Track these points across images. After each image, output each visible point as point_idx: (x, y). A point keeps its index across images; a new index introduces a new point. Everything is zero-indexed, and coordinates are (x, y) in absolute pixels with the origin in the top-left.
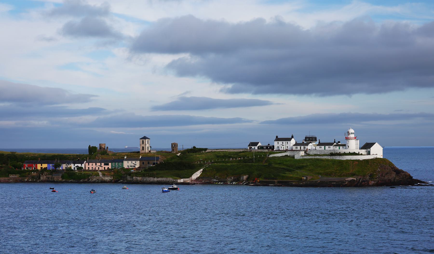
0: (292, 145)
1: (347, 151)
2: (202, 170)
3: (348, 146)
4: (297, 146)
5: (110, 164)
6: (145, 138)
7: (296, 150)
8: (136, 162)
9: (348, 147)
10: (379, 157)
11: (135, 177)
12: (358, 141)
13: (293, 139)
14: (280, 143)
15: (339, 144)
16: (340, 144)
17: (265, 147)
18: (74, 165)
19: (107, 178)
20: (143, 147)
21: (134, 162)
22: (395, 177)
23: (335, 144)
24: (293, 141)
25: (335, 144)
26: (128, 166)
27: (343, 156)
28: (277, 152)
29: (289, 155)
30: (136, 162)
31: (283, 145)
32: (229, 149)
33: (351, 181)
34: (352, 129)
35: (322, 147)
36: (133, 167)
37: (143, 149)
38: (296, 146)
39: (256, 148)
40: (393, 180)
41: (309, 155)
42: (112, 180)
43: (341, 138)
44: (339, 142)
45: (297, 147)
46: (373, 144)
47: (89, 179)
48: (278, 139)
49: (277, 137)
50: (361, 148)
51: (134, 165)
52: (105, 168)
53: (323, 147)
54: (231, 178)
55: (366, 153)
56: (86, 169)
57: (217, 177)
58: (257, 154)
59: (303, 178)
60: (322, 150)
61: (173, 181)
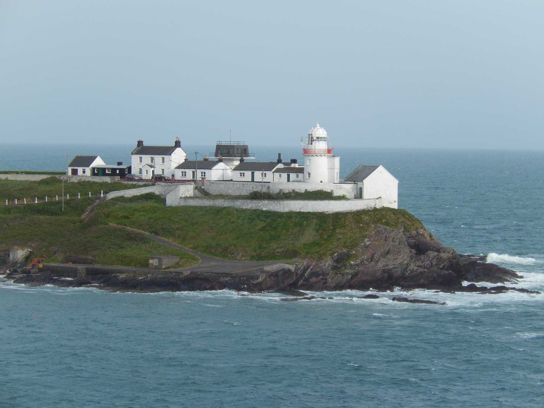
0: (174, 165)
1: (301, 187)
3: (309, 174)
4: (289, 174)
9: (309, 176)
10: (386, 205)
12: (337, 160)
14: (147, 159)
15: (293, 165)
16: (297, 166)
17: (110, 168)
23: (280, 166)
25: (280, 166)
27: (282, 202)
28: (132, 185)
29: (157, 193)
32: (369, 199)
33: (275, 275)
34: (321, 126)
38: (183, 170)
45: (185, 173)
46: (375, 168)
49: (140, 143)
53: (248, 175)
58: (84, 185)
59: (151, 261)
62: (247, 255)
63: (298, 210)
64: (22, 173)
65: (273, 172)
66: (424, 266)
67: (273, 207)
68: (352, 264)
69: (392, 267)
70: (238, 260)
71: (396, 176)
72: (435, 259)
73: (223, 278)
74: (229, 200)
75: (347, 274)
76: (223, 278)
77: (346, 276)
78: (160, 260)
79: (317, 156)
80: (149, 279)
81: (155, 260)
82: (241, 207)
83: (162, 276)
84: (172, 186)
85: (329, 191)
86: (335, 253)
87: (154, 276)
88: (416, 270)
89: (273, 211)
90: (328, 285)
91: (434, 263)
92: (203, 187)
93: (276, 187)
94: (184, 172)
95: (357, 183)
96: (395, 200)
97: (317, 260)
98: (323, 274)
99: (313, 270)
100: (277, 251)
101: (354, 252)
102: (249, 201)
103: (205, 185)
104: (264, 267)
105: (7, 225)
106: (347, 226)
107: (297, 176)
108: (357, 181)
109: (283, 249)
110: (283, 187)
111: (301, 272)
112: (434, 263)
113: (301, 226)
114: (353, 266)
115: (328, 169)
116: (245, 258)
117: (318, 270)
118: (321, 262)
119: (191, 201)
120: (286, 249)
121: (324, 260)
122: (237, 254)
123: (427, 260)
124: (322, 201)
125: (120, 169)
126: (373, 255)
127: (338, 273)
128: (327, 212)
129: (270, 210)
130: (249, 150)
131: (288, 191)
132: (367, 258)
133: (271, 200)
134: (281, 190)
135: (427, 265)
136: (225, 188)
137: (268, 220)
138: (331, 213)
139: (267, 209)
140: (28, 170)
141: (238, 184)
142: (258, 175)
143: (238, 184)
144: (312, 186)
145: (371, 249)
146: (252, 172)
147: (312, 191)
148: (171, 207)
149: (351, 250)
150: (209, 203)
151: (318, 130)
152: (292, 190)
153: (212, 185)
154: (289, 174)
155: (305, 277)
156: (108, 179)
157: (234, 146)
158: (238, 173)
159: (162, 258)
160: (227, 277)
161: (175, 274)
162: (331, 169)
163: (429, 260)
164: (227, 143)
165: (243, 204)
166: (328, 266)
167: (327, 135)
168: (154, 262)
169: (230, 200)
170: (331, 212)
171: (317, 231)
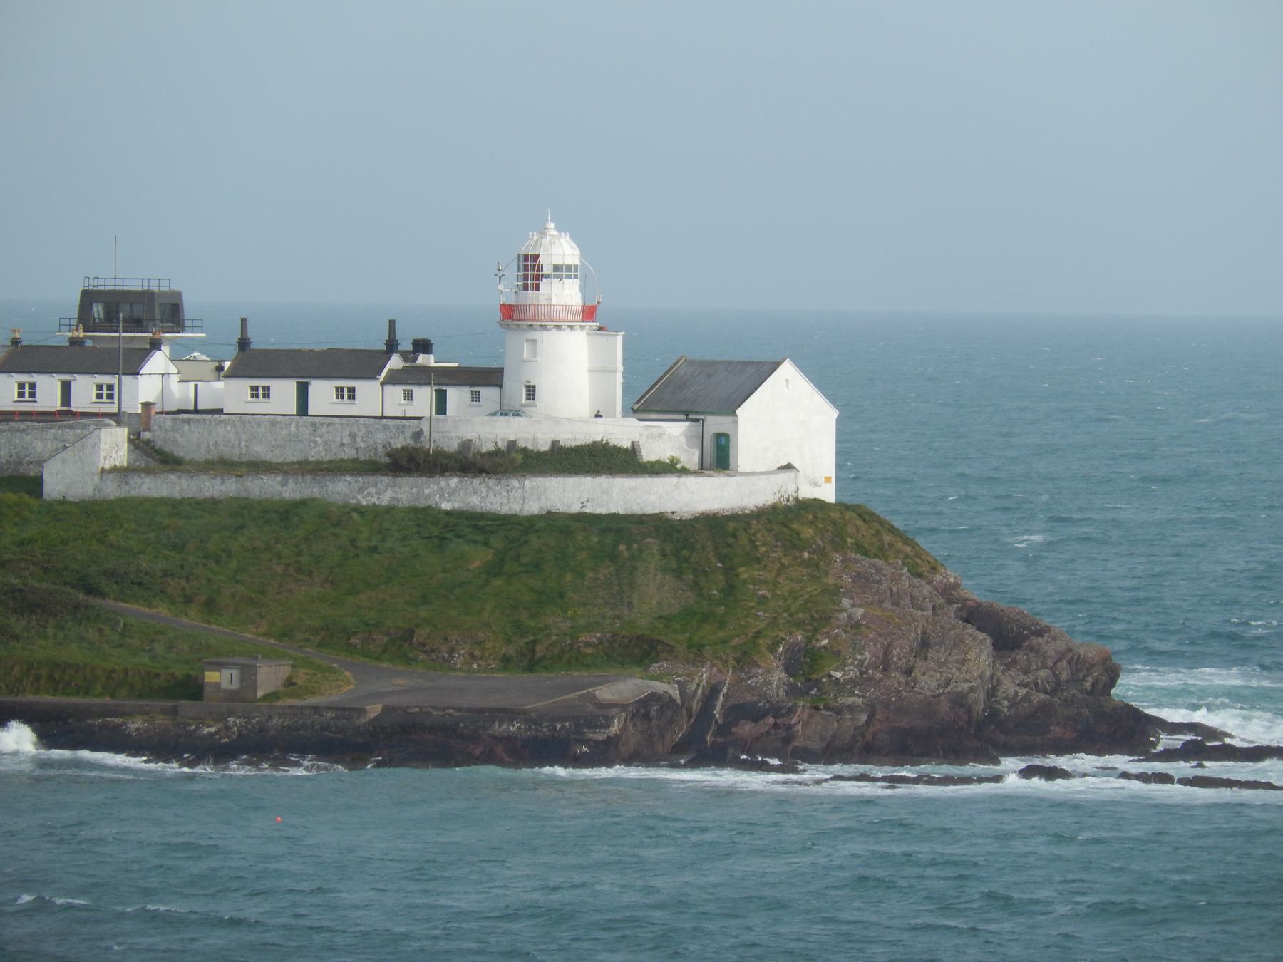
4: (36, 378)
7: (95, 409)
10: (807, 493)
15: (422, 359)
22: (992, 677)
25: (395, 362)
27: (514, 483)
32: (754, 474)
33: (645, 709)
35: (277, 386)
38: (25, 378)
40: (978, 702)
41: (166, 461)
44: (423, 346)
45: (33, 386)
53: (284, 392)
55: (690, 458)
59: (211, 676)
60: (274, 420)
62: (487, 654)
63: (575, 509)
65: (382, 384)
66: (1036, 684)
67: (482, 497)
68: (836, 678)
69: (966, 686)
70: (460, 670)
71: (832, 398)
72: (1065, 662)
73: (500, 726)
74: (303, 475)
75: (851, 708)
76: (500, 726)
77: (848, 717)
78: (248, 673)
79: (533, 328)
80: (234, 732)
81: (226, 673)
82: (353, 501)
83: (286, 724)
84: (27, 434)
85: (626, 444)
86: (778, 643)
87: (254, 722)
88: (1026, 698)
89: (472, 513)
90: (796, 744)
91: (1064, 676)
92: (146, 435)
93: (447, 434)
94: (105, 387)
95: (702, 417)
96: (828, 475)
97: (734, 667)
98: (776, 711)
99: (732, 699)
100: (583, 639)
101: (825, 642)
102: (385, 480)
103: (155, 427)
104: (596, 690)
106: (765, 559)
107: (409, 396)
108: (702, 413)
109: (599, 635)
110: (473, 434)
111: (699, 705)
112: (1064, 676)
113: (614, 557)
114: (844, 684)
115: (589, 371)
116: (481, 663)
117: (749, 698)
118: (748, 673)
119: (147, 480)
120: (608, 635)
121: (759, 667)
122: (452, 651)
123: (1037, 665)
124: (655, 479)
126: (887, 650)
127: (822, 707)
128: (673, 513)
129: (470, 510)
130: (184, 306)
131: (491, 447)
132: (870, 659)
133: (470, 475)
134: (466, 444)
135: (1042, 681)
136: (240, 439)
137: (496, 541)
138: (687, 516)
139: (457, 505)
141: (293, 425)
142: (322, 394)
143: (293, 425)
145: (871, 633)
146: (297, 383)
147: (574, 444)
148: (63, 502)
149: (814, 635)
150: (223, 488)
151: (557, 241)
152: (506, 444)
153: (186, 428)
154: (444, 388)
155: (717, 722)
158: (244, 385)
159: (256, 666)
160: (511, 721)
161: (334, 715)
162: (600, 371)
163: (1044, 666)
164: (156, 283)
165: (360, 490)
166: (778, 687)
167: (583, 255)
168: (220, 678)
169: (309, 478)
170: (686, 514)
171: (678, 573)
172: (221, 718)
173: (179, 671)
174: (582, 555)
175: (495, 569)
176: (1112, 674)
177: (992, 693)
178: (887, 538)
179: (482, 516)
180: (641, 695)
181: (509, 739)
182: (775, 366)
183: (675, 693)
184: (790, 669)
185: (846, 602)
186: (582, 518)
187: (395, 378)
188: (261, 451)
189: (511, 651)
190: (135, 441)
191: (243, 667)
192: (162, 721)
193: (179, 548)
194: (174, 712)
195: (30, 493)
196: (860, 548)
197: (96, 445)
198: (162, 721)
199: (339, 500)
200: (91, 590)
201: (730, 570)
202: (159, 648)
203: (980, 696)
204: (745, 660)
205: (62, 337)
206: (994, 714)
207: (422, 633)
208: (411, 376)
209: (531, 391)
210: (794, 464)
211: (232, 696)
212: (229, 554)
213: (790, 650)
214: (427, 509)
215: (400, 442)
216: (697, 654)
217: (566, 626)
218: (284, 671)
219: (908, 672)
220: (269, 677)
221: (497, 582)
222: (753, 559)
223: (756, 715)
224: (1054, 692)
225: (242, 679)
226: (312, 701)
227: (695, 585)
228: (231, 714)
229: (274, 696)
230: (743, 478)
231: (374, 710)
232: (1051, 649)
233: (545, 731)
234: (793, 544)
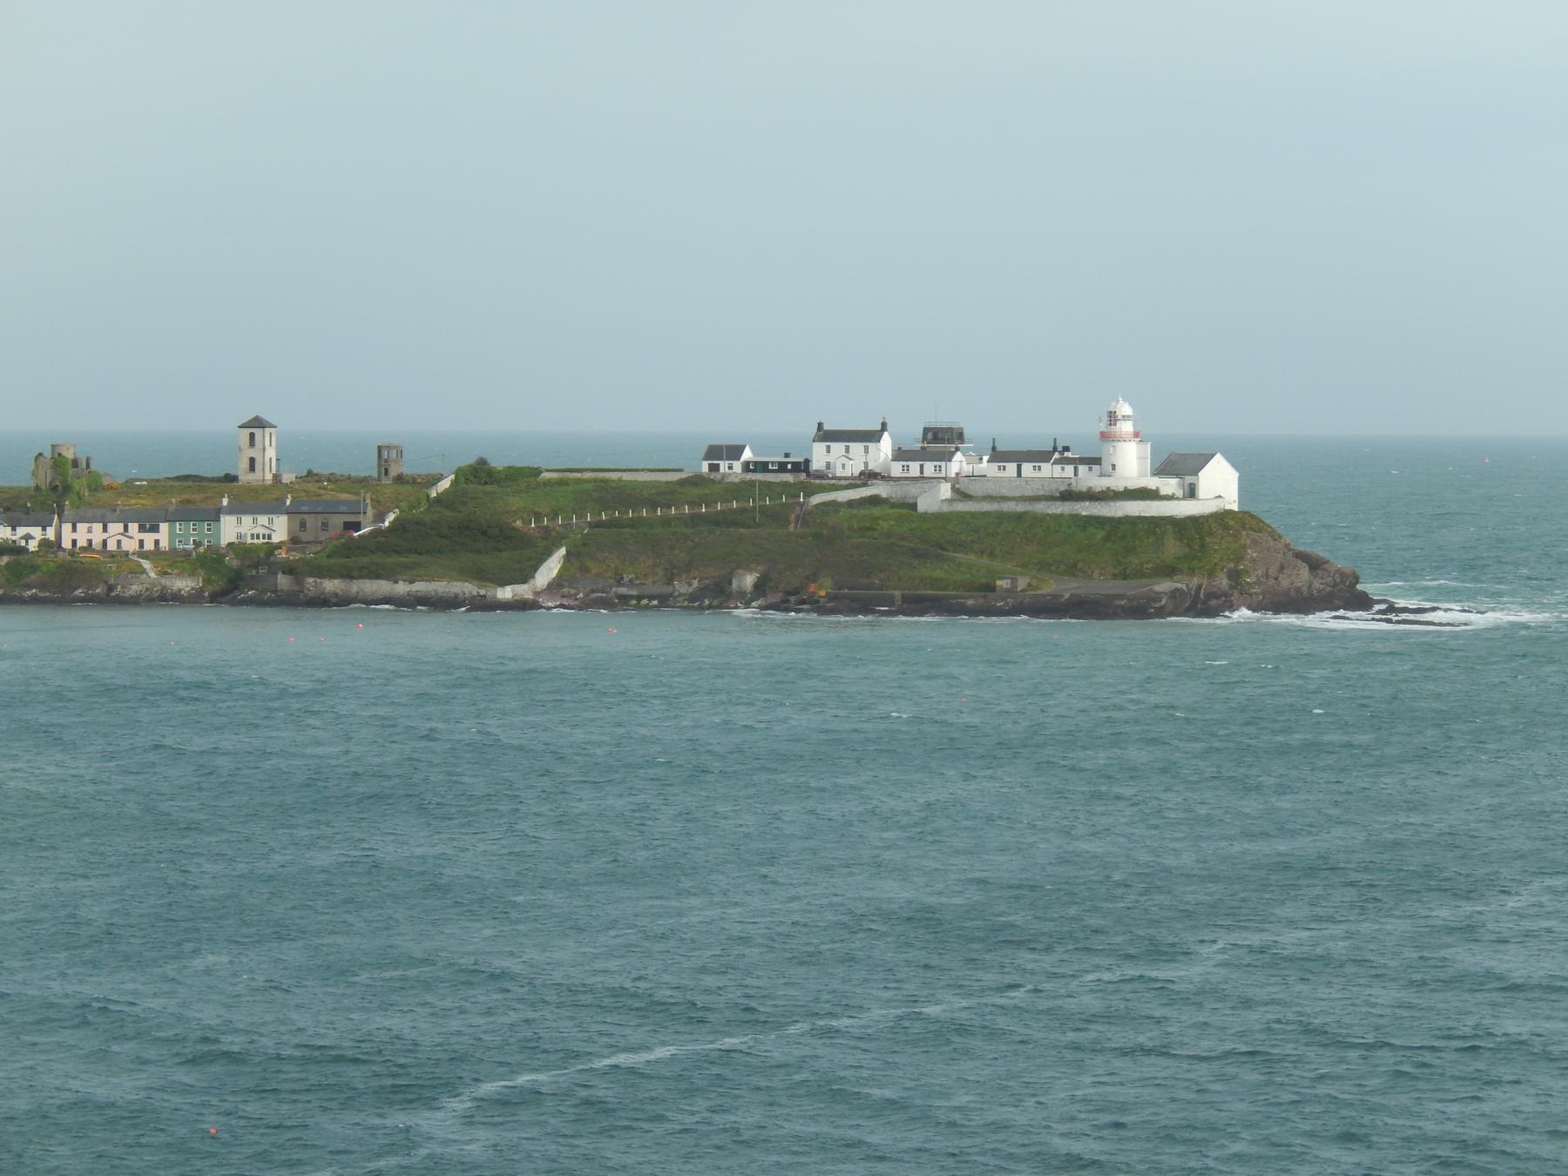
1: (1099, 483)
2: (563, 551)
4: (909, 463)
5: (164, 527)
6: (258, 423)
8: (271, 521)
11: (311, 580)
13: (886, 433)
14: (838, 448)
15: (1066, 454)
18: (14, 529)
19: (184, 584)
20: (252, 461)
21: (263, 519)
24: (886, 445)
25: (1056, 456)
26: (240, 536)
27: (1112, 504)
29: (884, 495)
30: (271, 521)
31: (850, 456)
33: (1174, 594)
36: (264, 538)
37: (252, 468)
38: (904, 463)
39: (737, 466)
41: (965, 496)
42: (201, 590)
43: (1077, 428)
44: (1066, 449)
47: (111, 588)
48: (826, 436)
49: (820, 425)
50: (1161, 470)
51: (267, 532)
52: (141, 542)
53: (1011, 468)
54: (690, 585)
55: (1180, 493)
56: (109, 548)
57: (631, 581)
59: (999, 583)
60: (1010, 480)
61: (475, 593)
63: (1137, 514)
64: (642, 470)
71: (1235, 465)
75: (1256, 594)
78: (1014, 581)
81: (1005, 581)
85: (1154, 488)
88: (1324, 589)
91: (1338, 580)
92: (957, 486)
98: (1225, 595)
105: (693, 541)
107: (1063, 469)
112: (1338, 580)
113: (1154, 533)
122: (1092, 572)
125: (793, 463)
126: (1267, 569)
134: (1090, 488)
137: (1106, 527)
140: (657, 467)
142: (1027, 468)
144: (1117, 483)
148: (926, 513)
156: (788, 478)
157: (952, 429)
158: (996, 465)
162: (1141, 458)
168: (1003, 584)
171: (1181, 540)
172: (1004, 599)
173: (984, 581)
174: (1142, 533)
175: (1106, 539)
176: (1357, 580)
177: (1310, 587)
178: (1261, 525)
179: (1099, 517)
180: (1044, 625)
181: (1121, 607)
182: (1213, 456)
183: (1185, 588)
184: (1230, 577)
185: (1249, 551)
186: (1139, 518)
187: (1057, 462)
188: (1005, 492)
189: (1116, 571)
190: (953, 488)
191: (1012, 579)
192: (981, 601)
193: (977, 531)
194: (985, 597)
195: (912, 510)
196: (1251, 529)
197: (939, 491)
198: (981, 601)
199: (1039, 511)
200: (943, 549)
201: (1202, 539)
202: (974, 572)
203: (1305, 588)
204: (1211, 574)
205: (918, 446)
206: (1311, 595)
207: (1080, 565)
208: (1064, 461)
209: (1114, 467)
210: (265, 416)
211: (1008, 591)
212: (997, 534)
213: (1229, 570)
214: (1076, 515)
215: (1063, 488)
216: (1192, 572)
217: (1137, 562)
218: (1027, 580)
219: (1276, 579)
220: (1022, 583)
221: (1109, 544)
222: (1211, 534)
223: (1217, 597)
224: (1333, 587)
225: (1012, 583)
226: (1039, 592)
227: (1188, 545)
228: (1008, 597)
229: (1024, 590)
230: (1177, 502)
231: (1067, 595)
232: (1332, 569)
233: (1135, 603)
234: (1226, 528)
